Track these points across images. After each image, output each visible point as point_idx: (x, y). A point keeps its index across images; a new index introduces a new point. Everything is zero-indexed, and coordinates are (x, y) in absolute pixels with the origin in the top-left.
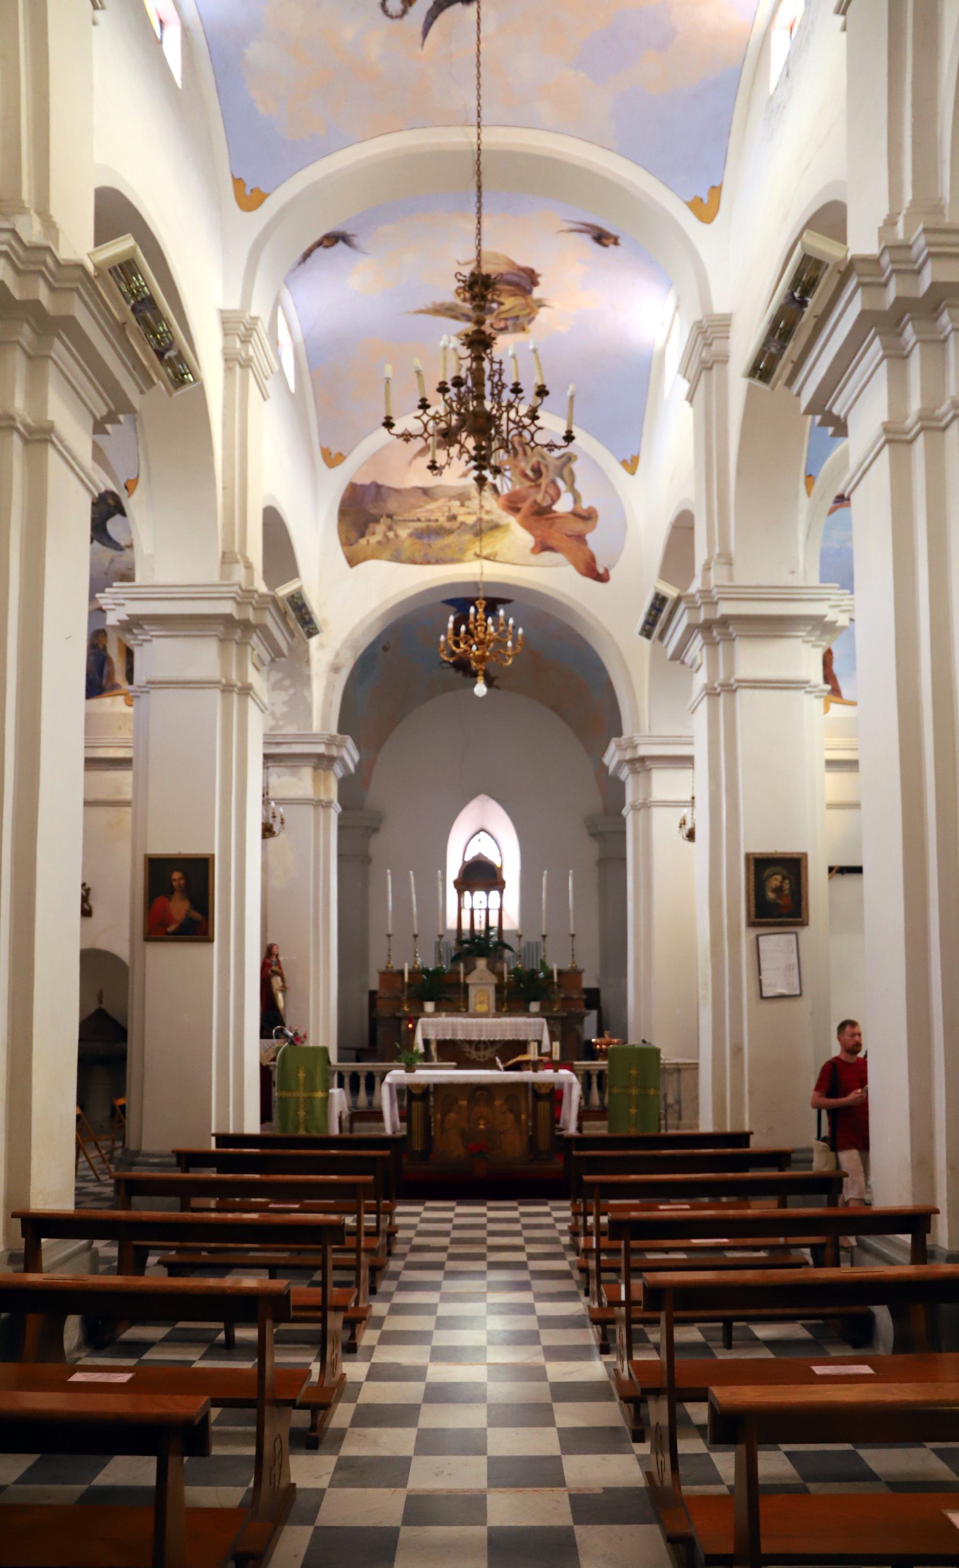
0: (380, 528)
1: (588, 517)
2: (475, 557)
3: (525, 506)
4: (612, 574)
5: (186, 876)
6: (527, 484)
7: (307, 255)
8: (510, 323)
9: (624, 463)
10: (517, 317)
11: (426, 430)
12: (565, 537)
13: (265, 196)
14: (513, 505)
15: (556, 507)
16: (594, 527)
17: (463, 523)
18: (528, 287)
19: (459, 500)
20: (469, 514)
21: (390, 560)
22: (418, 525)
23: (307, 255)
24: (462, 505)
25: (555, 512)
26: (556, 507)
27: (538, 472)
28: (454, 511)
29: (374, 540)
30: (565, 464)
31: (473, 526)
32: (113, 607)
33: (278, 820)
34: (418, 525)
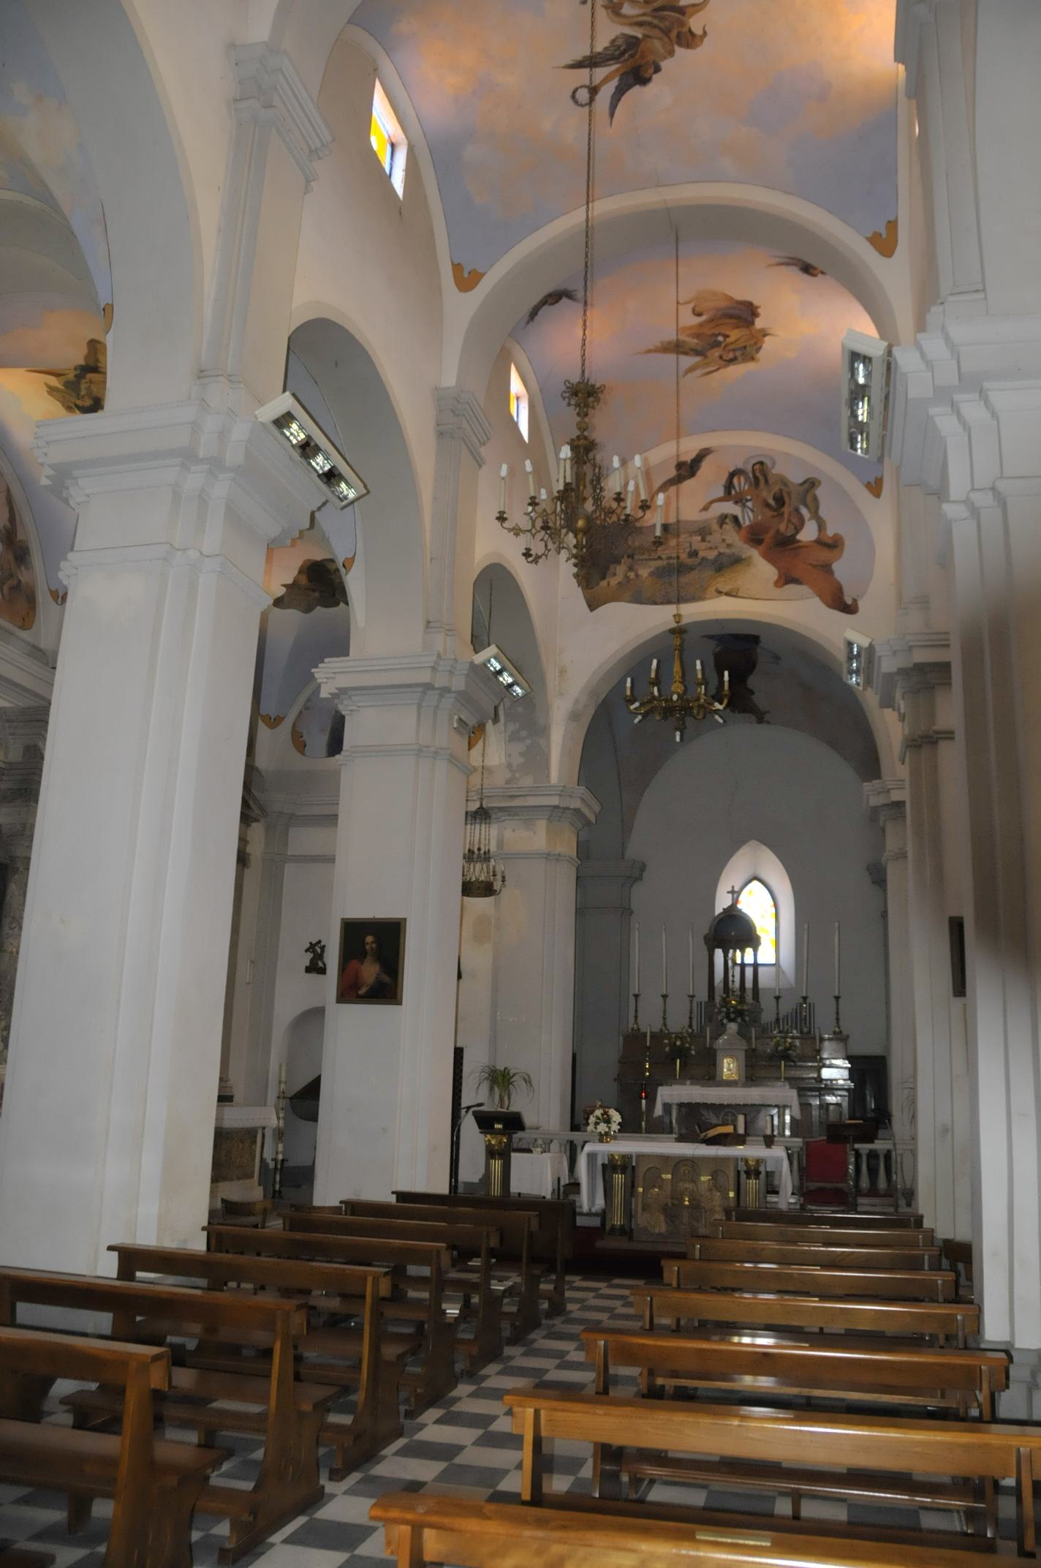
0: (621, 570)
1: (834, 545)
2: (717, 594)
3: (768, 538)
4: (862, 604)
5: (378, 940)
6: (769, 513)
7: (534, 313)
8: (738, 353)
9: (868, 486)
10: (745, 347)
11: (534, 526)
12: (810, 567)
13: (483, 275)
14: (755, 537)
15: (799, 537)
16: (840, 556)
17: (703, 559)
18: (749, 319)
19: (700, 535)
20: (711, 548)
21: (630, 602)
22: (659, 563)
23: (534, 313)
24: (703, 540)
25: (799, 541)
26: (799, 537)
27: (780, 500)
28: (694, 547)
29: (614, 581)
30: (808, 491)
31: (715, 560)
32: (325, 680)
33: (499, 877)
34: (659, 563)
